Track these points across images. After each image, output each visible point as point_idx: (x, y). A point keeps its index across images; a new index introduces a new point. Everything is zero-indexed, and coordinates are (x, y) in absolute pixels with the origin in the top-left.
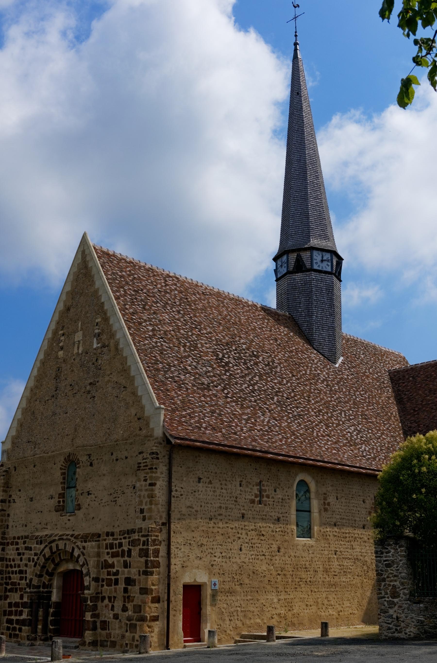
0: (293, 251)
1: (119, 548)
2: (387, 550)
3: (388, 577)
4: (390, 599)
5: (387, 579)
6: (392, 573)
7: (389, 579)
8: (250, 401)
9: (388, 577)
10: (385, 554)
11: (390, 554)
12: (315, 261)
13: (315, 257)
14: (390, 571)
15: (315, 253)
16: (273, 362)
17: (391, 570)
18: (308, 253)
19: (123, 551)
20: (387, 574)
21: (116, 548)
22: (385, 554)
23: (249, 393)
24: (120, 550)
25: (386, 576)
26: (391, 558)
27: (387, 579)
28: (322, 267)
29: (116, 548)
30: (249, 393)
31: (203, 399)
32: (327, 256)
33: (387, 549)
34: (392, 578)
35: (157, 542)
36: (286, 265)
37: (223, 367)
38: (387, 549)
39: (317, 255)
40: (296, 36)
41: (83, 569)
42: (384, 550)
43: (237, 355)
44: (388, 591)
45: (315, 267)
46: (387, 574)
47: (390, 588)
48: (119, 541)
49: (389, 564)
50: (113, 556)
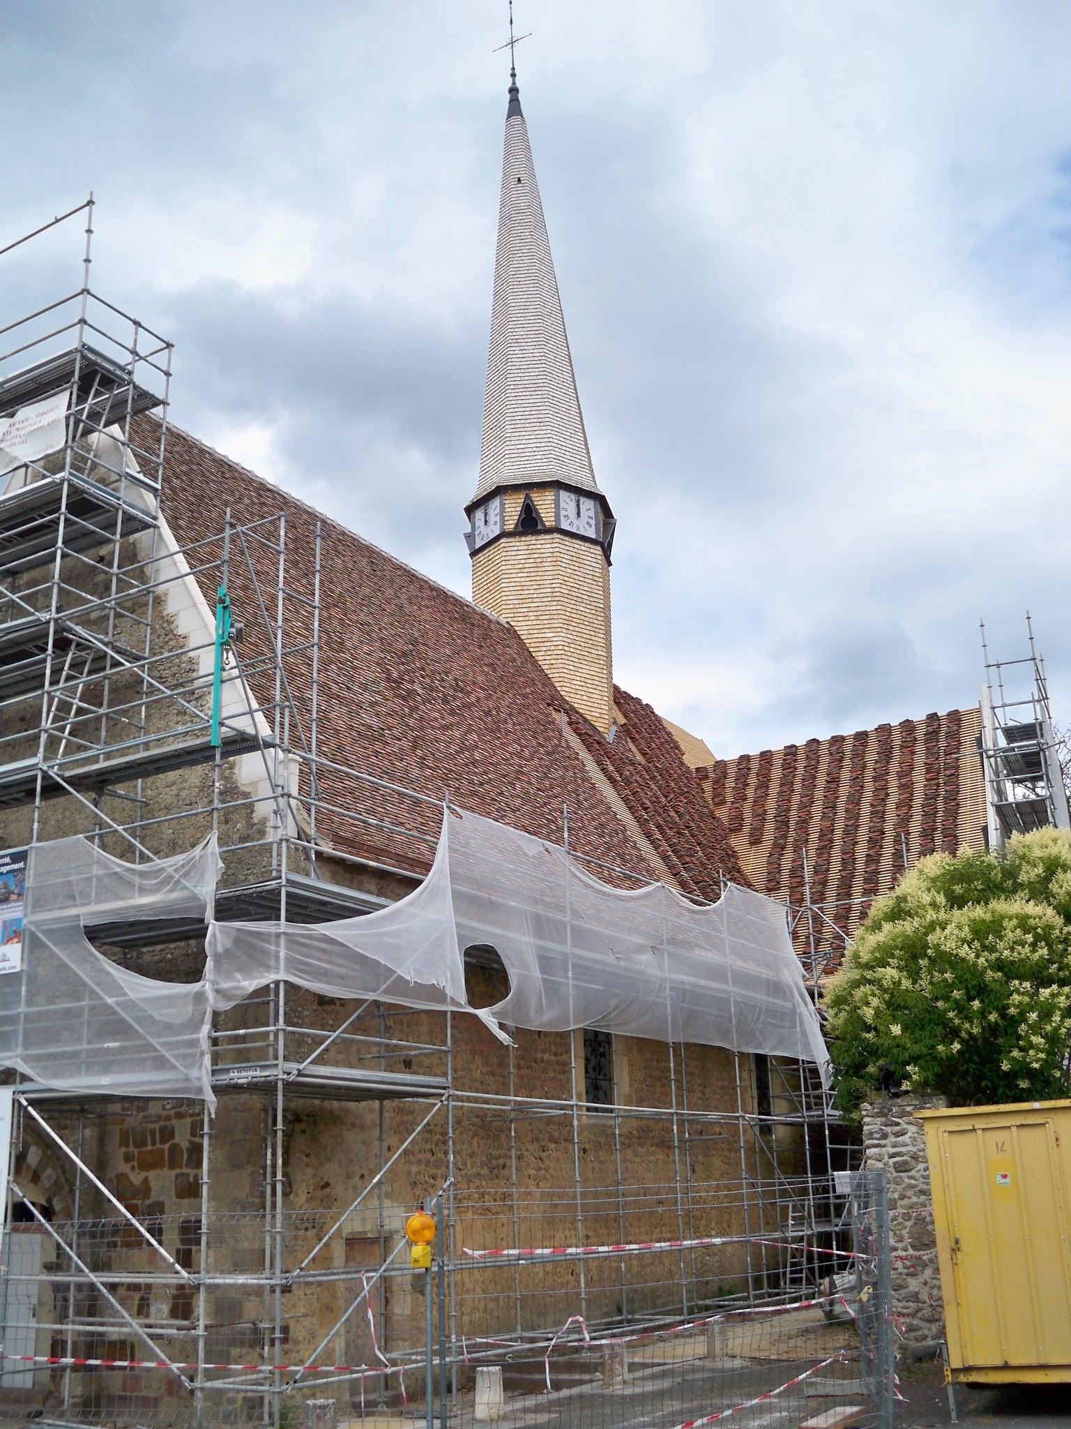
0: (515, 488)
1: (163, 1141)
2: (897, 1128)
3: (902, 1197)
4: (911, 1251)
5: (900, 1203)
6: (914, 1186)
7: (906, 1201)
8: (471, 782)
9: (902, 1197)
10: (892, 1139)
11: (906, 1138)
12: (563, 513)
13: (562, 504)
14: (907, 1180)
15: (564, 495)
16: (498, 709)
17: (909, 1177)
18: (549, 496)
19: (175, 1149)
20: (900, 1188)
21: (153, 1143)
22: (892, 1139)
23: (466, 765)
24: (166, 1146)
25: (896, 1195)
26: (909, 1148)
27: (900, 1203)
28: (578, 528)
29: (153, 1143)
30: (466, 765)
31: (374, 760)
32: (588, 505)
33: (898, 1124)
34: (914, 1199)
35: (1024, 1084)
36: (498, 519)
37: (404, 698)
38: (898, 1124)
39: (568, 500)
40: (513, 75)
41: (55, 1202)
42: (888, 1129)
43: (428, 681)
44: (905, 1232)
45: (564, 525)
46: (900, 1188)
47: (909, 1224)
48: (162, 1123)
49: (905, 1163)
50: (144, 1166)
